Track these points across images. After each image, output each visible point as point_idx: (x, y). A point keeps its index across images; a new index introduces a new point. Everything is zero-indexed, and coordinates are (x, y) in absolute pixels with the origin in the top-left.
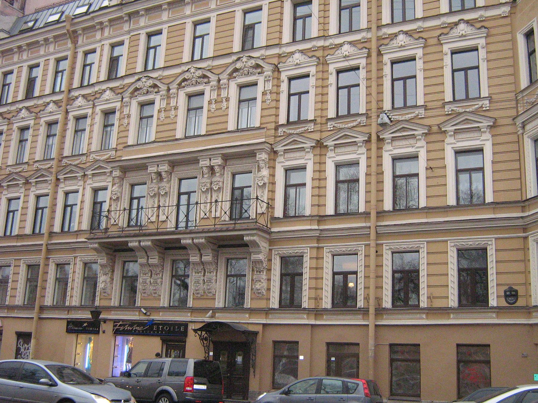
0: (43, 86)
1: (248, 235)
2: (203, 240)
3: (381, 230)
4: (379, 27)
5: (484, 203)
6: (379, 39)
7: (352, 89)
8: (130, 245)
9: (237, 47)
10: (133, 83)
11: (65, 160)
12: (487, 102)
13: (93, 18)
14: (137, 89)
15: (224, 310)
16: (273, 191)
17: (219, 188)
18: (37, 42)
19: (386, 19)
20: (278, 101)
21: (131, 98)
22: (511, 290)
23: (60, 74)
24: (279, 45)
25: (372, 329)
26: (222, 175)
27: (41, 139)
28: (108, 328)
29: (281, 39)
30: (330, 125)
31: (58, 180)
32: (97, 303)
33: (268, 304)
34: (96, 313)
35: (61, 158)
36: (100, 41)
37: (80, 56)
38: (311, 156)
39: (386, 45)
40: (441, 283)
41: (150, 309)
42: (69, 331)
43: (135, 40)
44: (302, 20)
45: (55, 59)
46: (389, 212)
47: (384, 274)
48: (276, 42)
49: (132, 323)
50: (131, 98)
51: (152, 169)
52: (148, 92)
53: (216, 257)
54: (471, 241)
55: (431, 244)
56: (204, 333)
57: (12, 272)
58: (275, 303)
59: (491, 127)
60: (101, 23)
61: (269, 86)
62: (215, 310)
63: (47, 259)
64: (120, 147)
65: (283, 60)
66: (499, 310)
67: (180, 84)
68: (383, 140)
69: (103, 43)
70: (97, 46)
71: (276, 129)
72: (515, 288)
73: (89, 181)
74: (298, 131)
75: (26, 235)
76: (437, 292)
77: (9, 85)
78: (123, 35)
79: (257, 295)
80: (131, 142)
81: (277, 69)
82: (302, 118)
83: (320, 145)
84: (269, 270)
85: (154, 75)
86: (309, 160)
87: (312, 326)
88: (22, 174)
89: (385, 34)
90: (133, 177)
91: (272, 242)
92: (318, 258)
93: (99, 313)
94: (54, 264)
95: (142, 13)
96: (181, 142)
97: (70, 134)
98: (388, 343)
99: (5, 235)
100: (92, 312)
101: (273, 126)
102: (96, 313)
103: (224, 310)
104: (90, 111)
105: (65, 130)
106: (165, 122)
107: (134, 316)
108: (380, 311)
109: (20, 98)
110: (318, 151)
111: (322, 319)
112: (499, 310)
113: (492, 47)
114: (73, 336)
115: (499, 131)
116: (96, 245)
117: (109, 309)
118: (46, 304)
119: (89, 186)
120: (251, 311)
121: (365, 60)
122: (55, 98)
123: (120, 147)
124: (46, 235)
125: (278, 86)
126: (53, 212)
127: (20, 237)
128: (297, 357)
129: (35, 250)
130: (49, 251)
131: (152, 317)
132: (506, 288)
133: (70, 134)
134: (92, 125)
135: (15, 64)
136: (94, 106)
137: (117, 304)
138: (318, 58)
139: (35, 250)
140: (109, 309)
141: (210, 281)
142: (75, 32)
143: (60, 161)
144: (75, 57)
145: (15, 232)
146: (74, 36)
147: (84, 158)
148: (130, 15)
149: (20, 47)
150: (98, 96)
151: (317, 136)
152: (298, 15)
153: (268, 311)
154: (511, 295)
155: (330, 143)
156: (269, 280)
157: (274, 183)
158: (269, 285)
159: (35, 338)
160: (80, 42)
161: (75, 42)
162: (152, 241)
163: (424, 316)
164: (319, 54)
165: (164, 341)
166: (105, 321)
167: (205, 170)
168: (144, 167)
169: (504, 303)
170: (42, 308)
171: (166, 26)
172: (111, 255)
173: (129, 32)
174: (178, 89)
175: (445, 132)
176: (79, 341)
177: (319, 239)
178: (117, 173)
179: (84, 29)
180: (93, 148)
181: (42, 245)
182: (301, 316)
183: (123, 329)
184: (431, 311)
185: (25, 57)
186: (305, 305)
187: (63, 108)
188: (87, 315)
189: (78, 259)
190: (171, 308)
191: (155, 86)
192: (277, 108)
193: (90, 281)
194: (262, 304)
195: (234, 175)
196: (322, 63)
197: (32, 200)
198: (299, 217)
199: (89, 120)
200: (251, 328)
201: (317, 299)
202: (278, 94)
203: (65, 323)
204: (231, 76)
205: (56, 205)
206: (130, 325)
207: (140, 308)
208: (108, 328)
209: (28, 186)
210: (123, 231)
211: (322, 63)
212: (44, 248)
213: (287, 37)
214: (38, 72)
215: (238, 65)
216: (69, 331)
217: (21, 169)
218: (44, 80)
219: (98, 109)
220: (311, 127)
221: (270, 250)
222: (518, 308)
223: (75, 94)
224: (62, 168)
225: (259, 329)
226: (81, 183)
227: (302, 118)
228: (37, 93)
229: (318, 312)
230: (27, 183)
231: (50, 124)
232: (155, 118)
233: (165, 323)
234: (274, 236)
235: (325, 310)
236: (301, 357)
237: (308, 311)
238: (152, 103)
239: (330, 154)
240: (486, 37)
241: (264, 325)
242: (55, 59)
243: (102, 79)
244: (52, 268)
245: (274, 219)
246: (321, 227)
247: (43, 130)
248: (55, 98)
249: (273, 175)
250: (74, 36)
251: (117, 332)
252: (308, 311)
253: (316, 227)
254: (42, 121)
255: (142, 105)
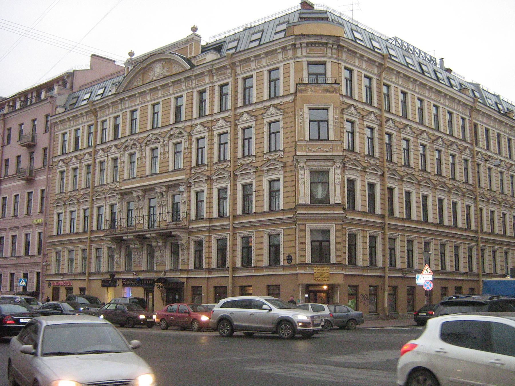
0: (124, 130)
1: (173, 231)
2: (155, 235)
3: (235, 226)
4: (236, 108)
5: (251, 213)
6: (235, 115)
7: (277, 134)
8: (147, 236)
9: (172, 120)
10: (125, 142)
11: (96, 189)
12: (282, 153)
13: (103, 102)
14: (126, 146)
15: (170, 271)
16: (190, 205)
17: (165, 204)
18: (77, 115)
19: (195, 116)
20: (191, 153)
21: (124, 151)
22: (289, 256)
23: (156, 115)
24: (191, 120)
25: (230, 279)
26: (167, 196)
27: (84, 175)
28: (120, 283)
29: (192, 115)
30: (215, 167)
31: (93, 200)
32: (115, 270)
33: (188, 266)
34: (112, 276)
35: (236, 159)
36: (109, 115)
37: (100, 124)
38: (205, 185)
39: (265, 113)
40: (261, 255)
41: (137, 272)
42: (103, 286)
43: (125, 115)
44: (274, 82)
45: (152, 104)
46: (240, 215)
47: (237, 249)
48: (190, 118)
49: (131, 280)
50: (169, 141)
51: (134, 194)
52: (132, 148)
53: (165, 243)
54: (274, 230)
55: (285, 230)
56: (159, 284)
57: (74, 254)
58: (192, 266)
59: (255, 172)
60: (107, 104)
61: (187, 145)
62: (166, 271)
63: (91, 246)
64: (121, 181)
65: (214, 123)
66: (284, 267)
67: (146, 143)
68: (237, 175)
69: (110, 116)
70: (80, 126)
71: (191, 170)
72: (291, 255)
73: (108, 201)
74: (200, 171)
75: (80, 233)
76: (259, 258)
77: (136, 119)
78: (79, 124)
79: (184, 263)
80: (125, 178)
81: (190, 135)
82: (250, 154)
83: (209, 179)
84: (188, 249)
85: (134, 137)
86: (204, 187)
87: (208, 278)
88: (204, 173)
89: (239, 113)
90: (127, 198)
91: (190, 233)
92: (210, 241)
93: (114, 276)
94: (240, 238)
95: (126, 99)
96: (149, 177)
97: (97, 172)
98: (239, 285)
99: (270, 209)
100: (110, 275)
101: (188, 168)
102: (112, 276)
103: (170, 271)
104: (106, 158)
105: (95, 170)
106: (164, 161)
107: (131, 276)
108: (235, 269)
109: (71, 151)
110: (209, 182)
111: (211, 274)
112: (284, 267)
113: (287, 120)
114: (105, 289)
115: (287, 169)
116: (109, 239)
117: (120, 273)
118: (92, 271)
119: (266, 178)
120: (182, 271)
121: (254, 122)
122: (89, 150)
123: (121, 181)
124: (89, 232)
125: (191, 144)
126: (92, 219)
127: (77, 234)
128: (201, 294)
129: (83, 241)
130: (91, 242)
131: (139, 276)
132: (287, 255)
133: (97, 172)
134: (80, 173)
135: (137, 105)
136: (108, 156)
137: (123, 270)
138: (208, 128)
139: (83, 241)
140: (120, 273)
141: (162, 256)
142: (95, 109)
143: (94, 189)
144: (97, 125)
145: (75, 231)
146: (95, 112)
147: (104, 187)
148: (122, 100)
149: (69, 118)
150: (109, 150)
151: (208, 173)
152: (272, 78)
153: (188, 271)
154: (290, 259)
155: (214, 178)
156: (189, 254)
157: (190, 201)
158: (188, 256)
159: (87, 290)
160: (99, 116)
161: (96, 116)
162: (134, 236)
163: (253, 271)
164: (209, 125)
165: (145, 289)
166: (119, 279)
167: (159, 195)
168: (153, 189)
169: (286, 263)
170: (90, 274)
171: (139, 106)
172: (165, 239)
173: (122, 110)
174: (169, 141)
175: (263, 170)
176: (125, 291)
177: (210, 231)
178: (119, 197)
179: (100, 108)
180: (109, 182)
181: (229, 224)
182: (251, 271)
183: (127, 283)
184: (257, 268)
185: (85, 120)
186: (204, 267)
187: (93, 157)
188: (108, 277)
189: (105, 246)
190: (148, 271)
191: (135, 144)
192: (191, 157)
193: (111, 257)
194: (185, 267)
195: (150, 199)
196: (211, 130)
197: (82, 212)
198: (278, 211)
199: (106, 164)
200: (182, 280)
201: (209, 263)
202: (191, 148)
203: (101, 281)
204: (169, 139)
205: (93, 215)
206: (129, 281)
207: (133, 271)
208: (120, 283)
209: (260, 173)
210: (168, 225)
211: (211, 130)
212: (88, 240)
213: (195, 115)
214: (158, 108)
215: (172, 133)
216: (103, 286)
217: (250, 161)
218: (124, 126)
219: (110, 157)
220: (206, 168)
221: (189, 238)
222: (292, 265)
223: (98, 148)
224: (94, 193)
225: (185, 280)
226: (104, 202)
227: (250, 154)
228: (183, 118)
229: (210, 271)
230: (65, 204)
231: (88, 166)
232: (183, 152)
233: (145, 279)
234: (190, 230)
235: (213, 269)
236: (203, 295)
237: (205, 270)
238: (180, 143)
239: (215, 184)
240: (283, 115)
241: (187, 278)
242: (152, 104)
243: (110, 139)
244: (94, 251)
245: (191, 221)
246: (211, 225)
247: (84, 170)
248: (89, 150)
249: (189, 196)
250: (95, 112)
251: (124, 285)
252: (205, 270)
253: (208, 225)
254: (71, 167)
255: (175, 144)
